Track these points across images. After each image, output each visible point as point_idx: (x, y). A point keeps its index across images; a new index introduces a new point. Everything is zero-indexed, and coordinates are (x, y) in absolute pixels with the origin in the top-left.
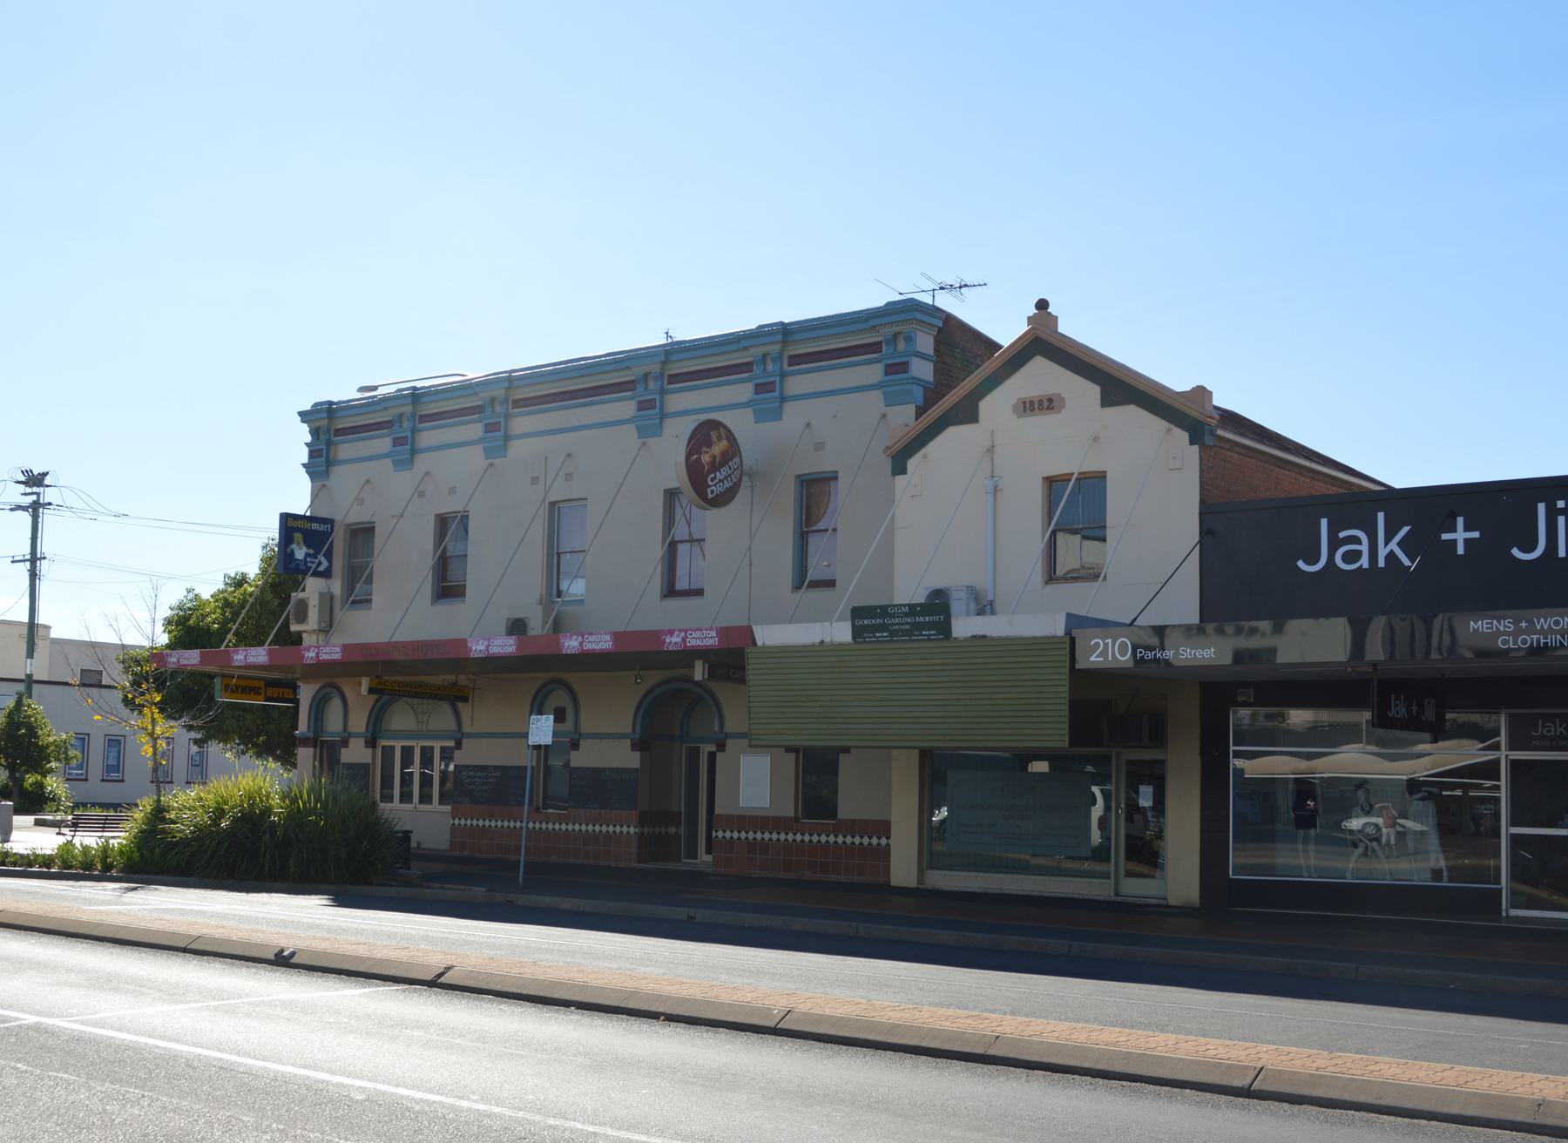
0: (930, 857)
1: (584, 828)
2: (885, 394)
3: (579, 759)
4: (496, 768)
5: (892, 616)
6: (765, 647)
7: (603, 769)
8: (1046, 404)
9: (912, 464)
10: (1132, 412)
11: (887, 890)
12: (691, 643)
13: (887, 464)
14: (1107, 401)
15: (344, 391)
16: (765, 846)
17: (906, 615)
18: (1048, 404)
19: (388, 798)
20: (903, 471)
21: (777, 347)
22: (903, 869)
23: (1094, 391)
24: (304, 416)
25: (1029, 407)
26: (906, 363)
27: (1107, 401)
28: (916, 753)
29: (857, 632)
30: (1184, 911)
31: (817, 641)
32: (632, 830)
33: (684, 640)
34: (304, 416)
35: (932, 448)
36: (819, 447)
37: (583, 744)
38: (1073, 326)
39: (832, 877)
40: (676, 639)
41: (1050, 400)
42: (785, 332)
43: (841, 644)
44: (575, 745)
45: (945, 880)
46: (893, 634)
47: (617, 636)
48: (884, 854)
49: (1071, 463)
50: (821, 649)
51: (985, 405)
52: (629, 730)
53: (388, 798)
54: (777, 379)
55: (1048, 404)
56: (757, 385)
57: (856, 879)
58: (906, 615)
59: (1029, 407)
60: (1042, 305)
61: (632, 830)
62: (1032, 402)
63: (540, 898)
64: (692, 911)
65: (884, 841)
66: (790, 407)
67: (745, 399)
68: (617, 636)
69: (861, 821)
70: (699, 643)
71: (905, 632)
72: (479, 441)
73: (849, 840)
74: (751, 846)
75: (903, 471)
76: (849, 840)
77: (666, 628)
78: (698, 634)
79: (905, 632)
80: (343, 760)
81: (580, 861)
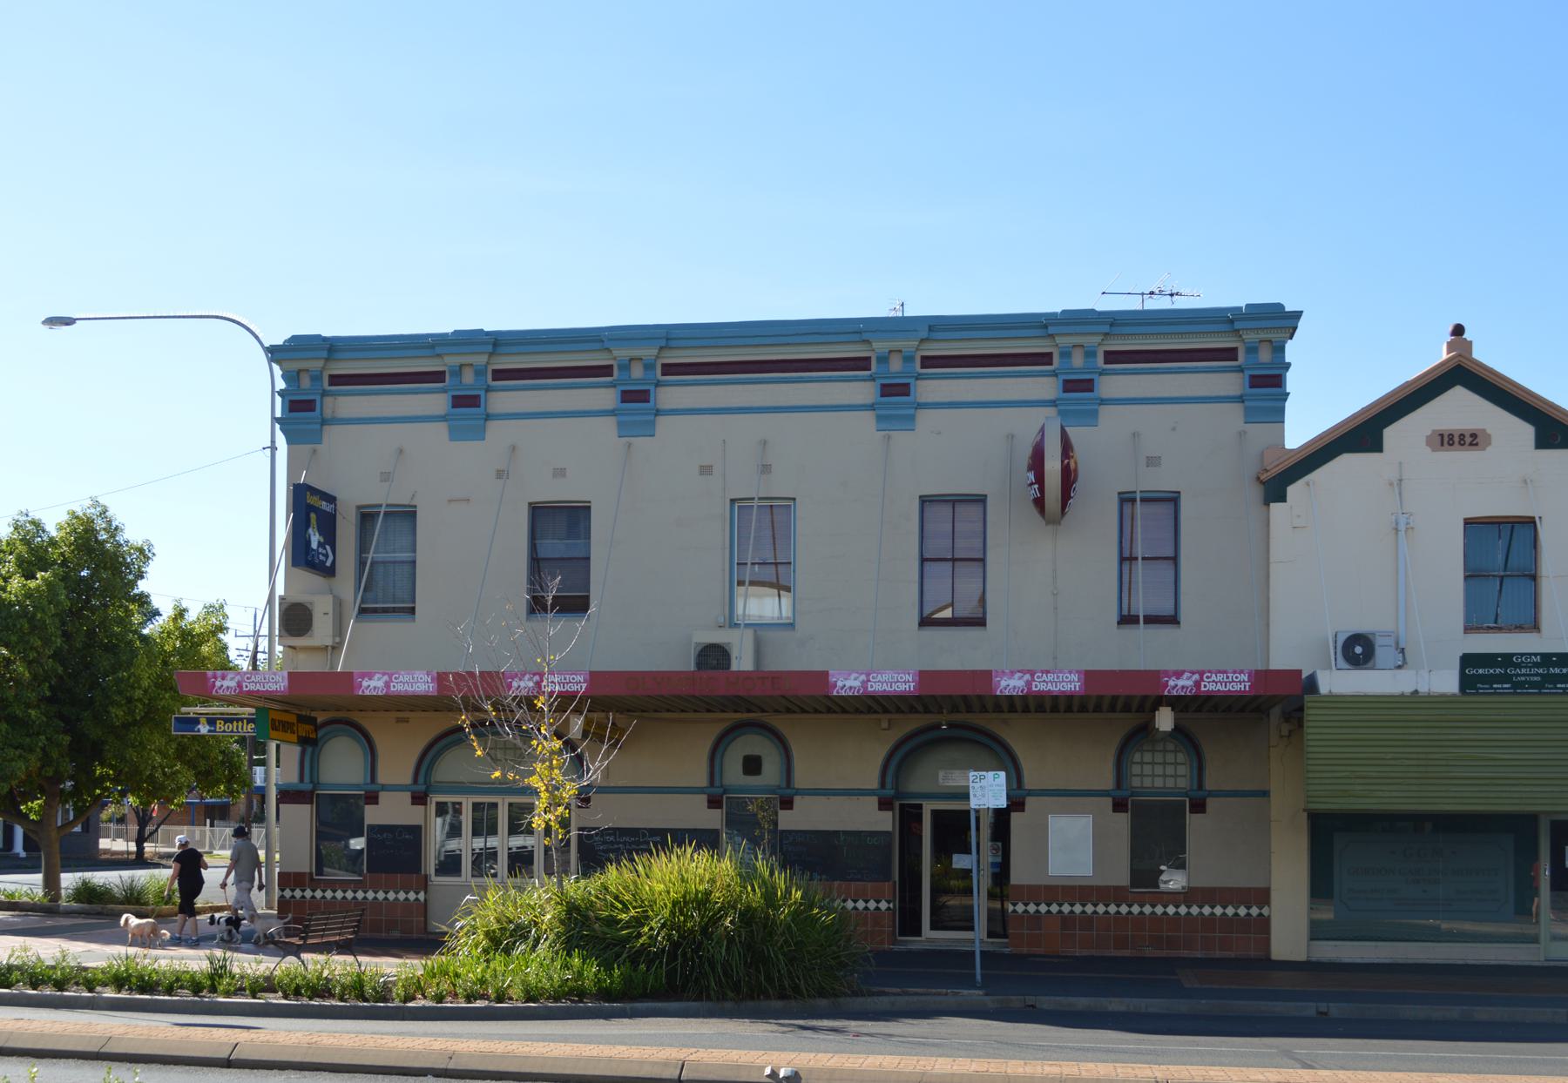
0: (1318, 932)
2: (1246, 409)
5: (1518, 666)
6: (1331, 695)
8: (1468, 440)
9: (1292, 490)
11: (1266, 963)
12: (1209, 686)
13: (1255, 493)
14: (1543, 442)
16: (1087, 921)
17: (1536, 665)
18: (1471, 440)
20: (1282, 498)
21: (320, 364)
22: (1289, 937)
23: (1527, 431)
24: (1297, 315)
25: (1447, 440)
27: (1543, 442)
29: (1466, 682)
31: (1408, 690)
32: (883, 905)
34: (1297, 315)
36: (1153, 461)
37: (798, 801)
38: (1488, 354)
39: (1185, 953)
41: (1474, 436)
42: (497, 342)
43: (1443, 695)
44: (787, 804)
45: (1330, 951)
46: (1516, 685)
47: (594, 677)
48: (1264, 924)
50: (1414, 701)
51: (1390, 434)
52: (874, 784)
54: (318, 398)
55: (1471, 440)
56: (907, 394)
57: (1218, 954)
58: (1536, 665)
59: (1447, 440)
60: (1458, 330)
61: (883, 905)
62: (1451, 436)
64: (1323, 1007)
65: (421, 896)
66: (493, 427)
67: (610, 407)
68: (1089, 676)
69: (1029, 887)
71: (1533, 685)
72: (612, 413)
74: (1067, 921)
75: (1282, 498)
76: (1207, 910)
77: (1172, 667)
78: (1220, 677)
79: (1533, 685)
80: (368, 821)
81: (1126, 953)
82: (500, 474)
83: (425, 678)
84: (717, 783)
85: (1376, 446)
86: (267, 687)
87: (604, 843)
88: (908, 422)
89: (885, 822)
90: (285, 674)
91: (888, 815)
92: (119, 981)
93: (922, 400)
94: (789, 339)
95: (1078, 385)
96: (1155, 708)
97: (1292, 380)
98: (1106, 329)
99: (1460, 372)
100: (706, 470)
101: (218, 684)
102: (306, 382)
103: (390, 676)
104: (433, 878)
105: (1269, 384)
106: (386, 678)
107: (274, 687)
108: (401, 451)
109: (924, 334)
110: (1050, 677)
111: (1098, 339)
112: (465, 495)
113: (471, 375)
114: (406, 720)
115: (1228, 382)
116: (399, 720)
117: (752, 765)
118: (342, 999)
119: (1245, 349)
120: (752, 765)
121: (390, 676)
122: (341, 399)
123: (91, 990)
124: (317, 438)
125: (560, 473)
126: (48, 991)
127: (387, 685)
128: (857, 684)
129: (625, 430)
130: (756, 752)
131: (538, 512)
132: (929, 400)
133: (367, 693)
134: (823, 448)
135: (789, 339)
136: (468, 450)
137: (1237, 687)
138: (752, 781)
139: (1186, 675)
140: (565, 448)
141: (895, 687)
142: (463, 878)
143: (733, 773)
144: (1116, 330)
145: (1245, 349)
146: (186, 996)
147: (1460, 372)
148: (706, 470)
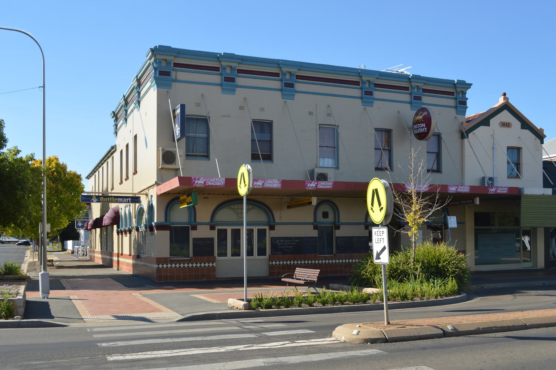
0: (477, 263)
1: (344, 261)
3: (338, 233)
4: (296, 238)
7: (353, 237)
10: (527, 132)
13: (458, 135)
14: (523, 127)
15: (153, 47)
18: (506, 125)
19: (223, 253)
26: (234, 78)
28: (543, 229)
30: (541, 270)
33: (496, 190)
34: (470, 85)
35: (476, 131)
40: (201, 182)
41: (509, 124)
47: (284, 182)
49: (514, 143)
51: (492, 121)
53: (223, 253)
55: (506, 125)
56: (169, 75)
63: (491, 285)
66: (238, 90)
68: (284, 182)
70: (323, 187)
73: (207, 265)
78: (501, 189)
82: (241, 108)
83: (277, 182)
84: (168, 220)
85: (488, 125)
86: (216, 184)
87: (280, 242)
88: (292, 97)
89: (315, 233)
90: (224, 179)
91: (316, 231)
92: (334, 301)
93: (239, 84)
94: (339, 73)
95: (227, 79)
96: (475, 197)
97: (469, 103)
98: (240, 61)
99: (507, 107)
100: (311, 113)
101: (196, 182)
102: (164, 64)
103: (264, 181)
104: (217, 257)
105: (462, 104)
106: (263, 182)
107: (219, 184)
108: (328, 106)
109: (378, 76)
110: (462, 187)
111: (422, 85)
112: (230, 115)
113: (230, 70)
114: (207, 198)
115: (451, 102)
116: (204, 198)
117: (325, 215)
118: (300, 306)
119: (456, 92)
120: (325, 215)
121: (264, 181)
122: (179, 73)
123: (311, 306)
124: (169, 86)
125: (262, 109)
126: (283, 309)
127: (263, 184)
128: (202, 182)
129: (284, 96)
130: (326, 210)
131: (256, 123)
132: (242, 85)
133: (197, 185)
134: (345, 108)
135: (339, 73)
136: (228, 98)
137: (328, 187)
138: (325, 220)
139: (260, 181)
140: (263, 100)
141: (326, 187)
142: (228, 257)
143: (320, 218)
144: (244, 62)
145: (456, 92)
146: (305, 307)
147: (507, 107)
148: (311, 113)
